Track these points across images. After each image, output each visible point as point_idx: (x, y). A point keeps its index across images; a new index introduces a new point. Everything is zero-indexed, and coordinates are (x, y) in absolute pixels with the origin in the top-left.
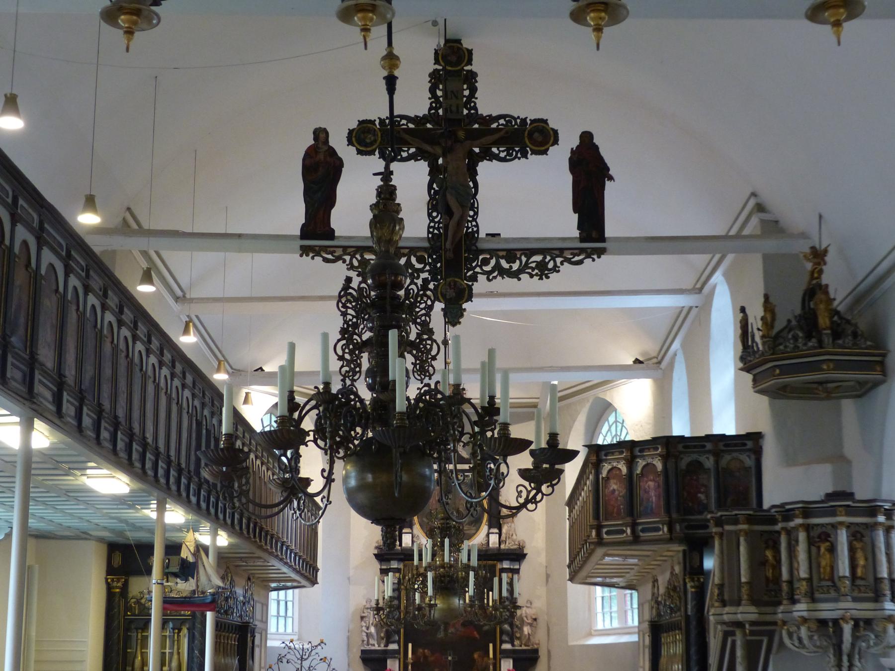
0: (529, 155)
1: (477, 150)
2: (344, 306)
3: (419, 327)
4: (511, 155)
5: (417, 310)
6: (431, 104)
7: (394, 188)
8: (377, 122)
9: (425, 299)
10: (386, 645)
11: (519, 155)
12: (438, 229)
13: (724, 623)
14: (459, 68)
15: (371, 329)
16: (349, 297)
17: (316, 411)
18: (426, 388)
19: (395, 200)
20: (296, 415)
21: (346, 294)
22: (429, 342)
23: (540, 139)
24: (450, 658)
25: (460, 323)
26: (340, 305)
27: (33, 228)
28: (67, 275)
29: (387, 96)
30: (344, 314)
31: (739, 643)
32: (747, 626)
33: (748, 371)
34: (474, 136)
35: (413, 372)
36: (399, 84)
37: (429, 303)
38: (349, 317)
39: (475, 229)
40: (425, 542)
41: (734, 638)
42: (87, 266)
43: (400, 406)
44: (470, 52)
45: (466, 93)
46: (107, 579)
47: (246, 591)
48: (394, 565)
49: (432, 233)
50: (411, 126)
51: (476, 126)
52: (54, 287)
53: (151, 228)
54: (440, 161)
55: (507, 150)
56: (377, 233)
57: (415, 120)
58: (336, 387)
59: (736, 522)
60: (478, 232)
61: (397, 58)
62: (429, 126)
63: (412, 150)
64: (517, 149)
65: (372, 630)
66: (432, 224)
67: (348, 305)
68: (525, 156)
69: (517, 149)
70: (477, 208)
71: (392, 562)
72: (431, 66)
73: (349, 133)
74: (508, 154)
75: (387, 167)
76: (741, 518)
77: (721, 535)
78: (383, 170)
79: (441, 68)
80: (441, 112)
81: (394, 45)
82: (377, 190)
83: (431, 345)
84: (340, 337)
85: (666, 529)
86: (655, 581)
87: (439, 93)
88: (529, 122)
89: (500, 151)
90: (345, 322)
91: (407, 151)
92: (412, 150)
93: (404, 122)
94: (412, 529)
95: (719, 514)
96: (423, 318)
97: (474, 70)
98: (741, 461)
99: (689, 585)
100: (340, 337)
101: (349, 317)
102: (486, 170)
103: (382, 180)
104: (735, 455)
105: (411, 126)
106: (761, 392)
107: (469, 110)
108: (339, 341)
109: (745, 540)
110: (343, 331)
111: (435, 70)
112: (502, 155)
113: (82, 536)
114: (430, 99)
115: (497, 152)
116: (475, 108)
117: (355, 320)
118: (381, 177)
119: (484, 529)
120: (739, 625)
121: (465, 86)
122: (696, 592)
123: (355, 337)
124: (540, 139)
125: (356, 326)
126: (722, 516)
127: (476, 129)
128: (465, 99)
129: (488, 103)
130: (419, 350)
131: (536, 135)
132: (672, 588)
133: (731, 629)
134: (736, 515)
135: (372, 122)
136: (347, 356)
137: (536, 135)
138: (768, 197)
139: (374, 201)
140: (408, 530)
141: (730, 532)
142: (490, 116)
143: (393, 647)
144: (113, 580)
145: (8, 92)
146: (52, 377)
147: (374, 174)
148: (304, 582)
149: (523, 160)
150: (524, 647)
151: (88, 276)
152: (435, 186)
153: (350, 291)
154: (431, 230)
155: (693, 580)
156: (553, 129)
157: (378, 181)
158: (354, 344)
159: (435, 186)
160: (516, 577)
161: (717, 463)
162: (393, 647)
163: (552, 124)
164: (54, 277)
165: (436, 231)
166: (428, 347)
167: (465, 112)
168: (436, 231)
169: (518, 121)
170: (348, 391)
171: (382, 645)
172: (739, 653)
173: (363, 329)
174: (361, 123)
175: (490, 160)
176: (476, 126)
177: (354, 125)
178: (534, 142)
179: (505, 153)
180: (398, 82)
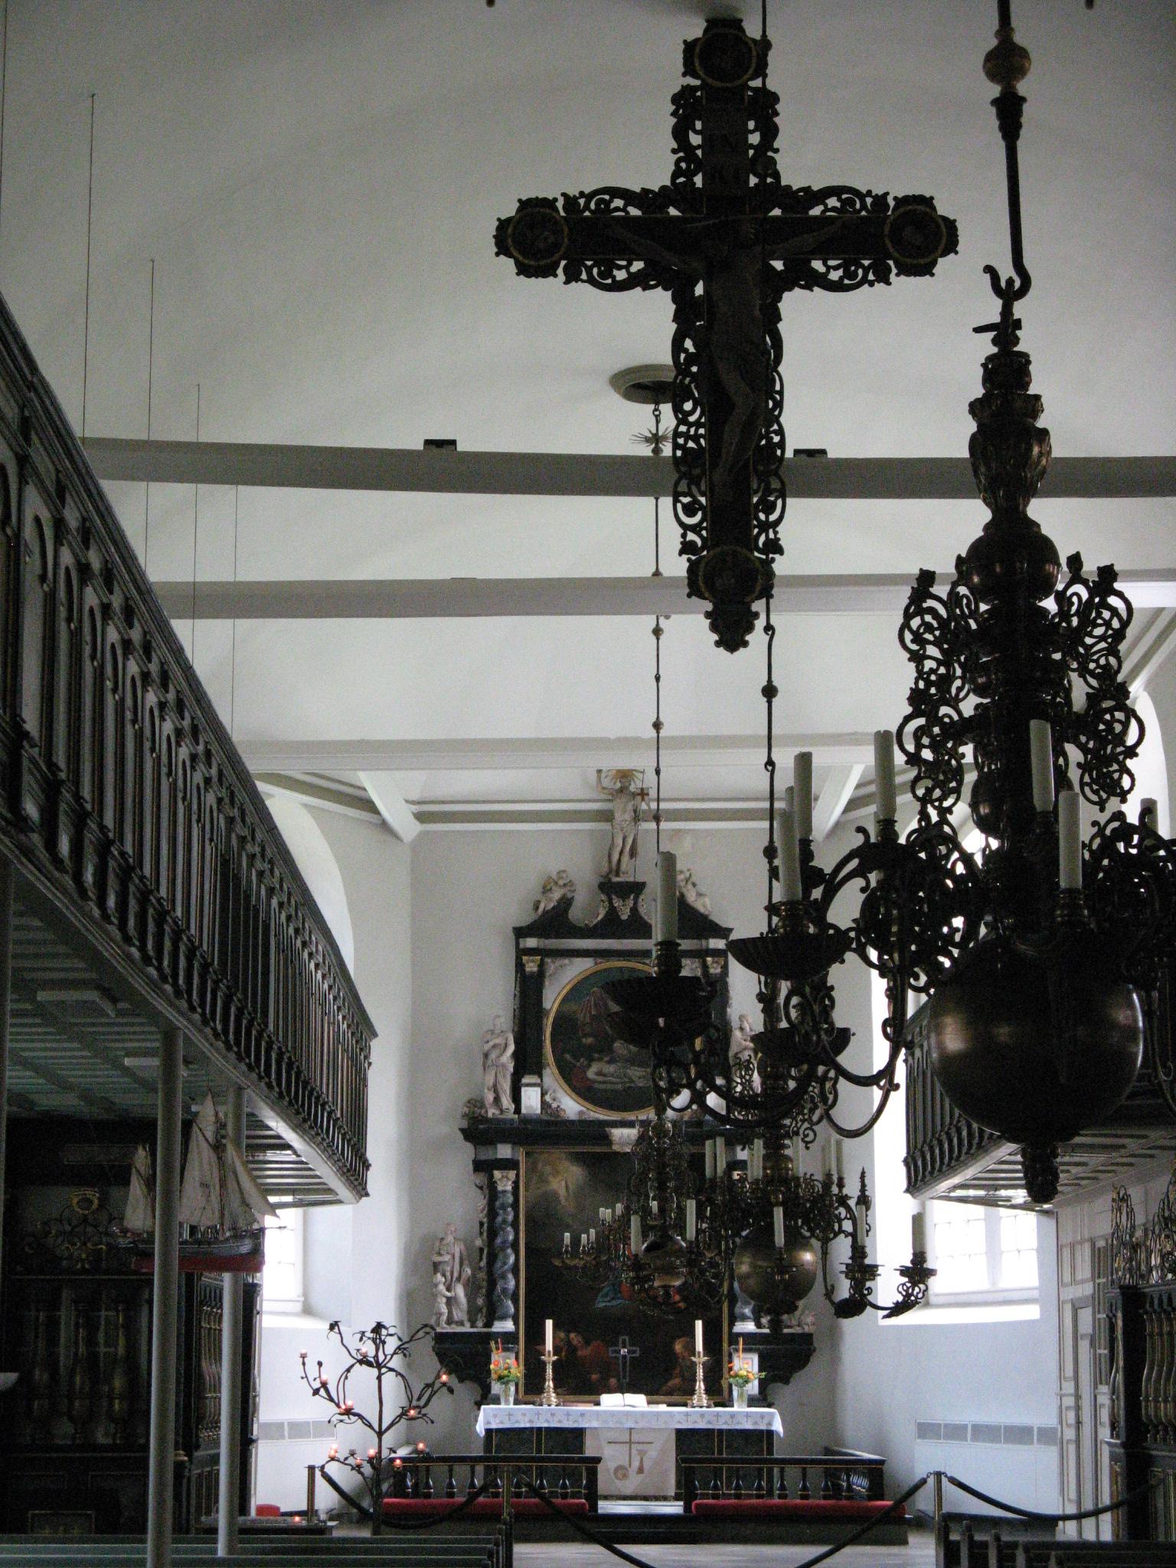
0: (893, 277)
1: (778, 265)
2: (918, 638)
3: (1094, 682)
4: (854, 275)
5: (1089, 641)
6: (677, 163)
7: (1024, 360)
8: (560, 204)
9: (1106, 614)
11: (871, 277)
12: (696, 438)
14: (740, 82)
15: (979, 691)
16: (928, 618)
17: (859, 882)
18: (1116, 824)
19: (1026, 385)
20: (817, 893)
21: (921, 612)
22: (1119, 715)
25: (745, 644)
26: (908, 636)
29: (1002, 144)
30: (917, 658)
34: (774, 236)
35: (1082, 784)
36: (1029, 114)
37: (1116, 624)
38: (929, 664)
39: (776, 439)
43: (1069, 875)
45: (755, 139)
48: (504, 1151)
49: (683, 447)
50: (634, 212)
51: (777, 212)
53: (152, 438)
54: (699, 290)
56: (989, 468)
57: (641, 199)
58: (907, 826)
60: (782, 445)
61: (1023, 53)
62: (673, 211)
63: (638, 266)
64: (866, 263)
65: (460, 1291)
66: (683, 428)
67: (929, 637)
69: (866, 263)
70: (781, 393)
71: (500, 1146)
72: (676, 79)
73: (498, 229)
74: (848, 274)
75: (1007, 311)
78: (997, 319)
79: (697, 82)
80: (698, 181)
81: (1014, 23)
82: (984, 365)
83: (1126, 725)
84: (909, 710)
87: (695, 140)
88: (892, 203)
89: (829, 268)
90: (920, 674)
91: (627, 268)
92: (638, 266)
93: (618, 203)
94: (541, 1076)
96: (1102, 661)
100: (909, 710)
101: (929, 664)
102: (799, 310)
103: (995, 342)
105: (634, 212)
108: (907, 719)
110: (917, 698)
111: (687, 90)
112: (835, 276)
114: (674, 151)
115: (822, 269)
116: (776, 175)
117: (942, 670)
118: (991, 335)
121: (751, 125)
123: (944, 710)
125: (945, 681)
127: (777, 217)
128: (751, 152)
129: (806, 158)
130: (1094, 734)
131: (908, 232)
135: (550, 203)
136: (927, 755)
137: (908, 232)
139: (979, 392)
140: (534, 1079)
142: (807, 190)
147: (977, 330)
149: (880, 287)
152: (688, 344)
153: (930, 603)
154: (681, 441)
156: (945, 219)
157: (985, 345)
158: (942, 725)
159: (688, 344)
163: (942, 209)
165: (691, 444)
166: (1118, 728)
167: (753, 181)
168: (691, 444)
169: (869, 200)
170: (936, 837)
171: (480, 1323)
173: (959, 689)
174: (524, 204)
175: (808, 287)
176: (777, 212)
177: (510, 210)
179: (840, 272)
180: (1026, 107)
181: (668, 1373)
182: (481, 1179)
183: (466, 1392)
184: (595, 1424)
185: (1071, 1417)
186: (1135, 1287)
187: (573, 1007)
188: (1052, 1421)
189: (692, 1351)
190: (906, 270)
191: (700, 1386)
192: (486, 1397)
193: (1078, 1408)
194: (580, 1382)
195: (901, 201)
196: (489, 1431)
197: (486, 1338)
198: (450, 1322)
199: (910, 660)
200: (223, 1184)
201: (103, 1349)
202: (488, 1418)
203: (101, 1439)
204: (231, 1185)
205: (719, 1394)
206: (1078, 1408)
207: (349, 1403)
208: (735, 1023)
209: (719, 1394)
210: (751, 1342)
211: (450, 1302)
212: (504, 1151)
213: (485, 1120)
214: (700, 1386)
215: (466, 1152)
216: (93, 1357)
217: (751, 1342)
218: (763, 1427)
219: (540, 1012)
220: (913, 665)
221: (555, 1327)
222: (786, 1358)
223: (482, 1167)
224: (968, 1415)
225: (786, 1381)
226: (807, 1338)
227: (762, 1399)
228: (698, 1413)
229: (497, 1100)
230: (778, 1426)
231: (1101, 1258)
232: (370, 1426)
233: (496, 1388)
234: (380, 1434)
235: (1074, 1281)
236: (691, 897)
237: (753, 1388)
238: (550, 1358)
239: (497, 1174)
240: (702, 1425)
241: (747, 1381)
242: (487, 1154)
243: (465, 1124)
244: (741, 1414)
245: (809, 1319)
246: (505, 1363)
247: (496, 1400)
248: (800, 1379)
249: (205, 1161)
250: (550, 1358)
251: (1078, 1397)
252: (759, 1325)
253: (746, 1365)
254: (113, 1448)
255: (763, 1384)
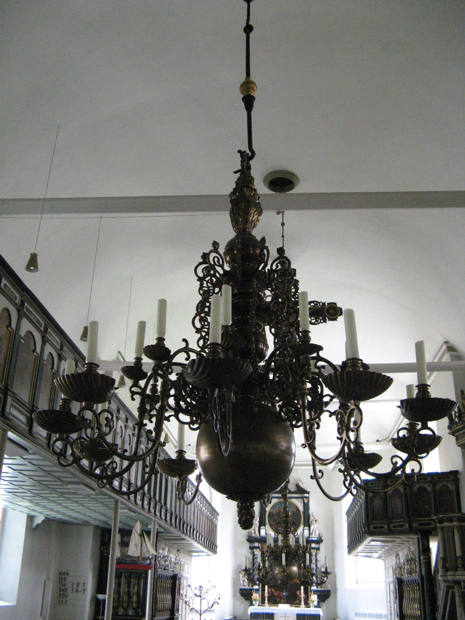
0: (327, 321)
4: (318, 321)
10: (252, 586)
13: (448, 581)
23: (333, 312)
24: (284, 594)
27: (17, 304)
28: (44, 343)
31: (457, 594)
32: (462, 584)
33: (453, 435)
36: (256, 104)
40: (272, 534)
41: (453, 590)
42: (61, 342)
44: (295, 270)
45: (293, 290)
46: (100, 548)
47: (176, 557)
48: (256, 544)
52: (33, 348)
55: (316, 319)
59: (451, 520)
68: (325, 321)
76: (454, 519)
77: (442, 528)
78: (240, 168)
85: (407, 526)
86: (397, 555)
88: (326, 304)
95: (441, 516)
97: (297, 279)
98: (447, 487)
99: (422, 558)
104: (444, 483)
106: (459, 446)
107: (295, 299)
109: (458, 531)
113: (86, 524)
119: (302, 527)
120: (458, 582)
122: (426, 562)
124: (333, 312)
126: (442, 517)
131: (331, 310)
132: (409, 561)
133: (451, 585)
134: (451, 516)
137: (331, 310)
138: (456, 342)
141: (448, 527)
143: (256, 587)
144: (104, 549)
145: (33, 252)
146: (26, 407)
148: (210, 553)
150: (322, 589)
151: (62, 349)
155: (425, 555)
160: (318, 551)
161: (434, 488)
162: (256, 587)
163: (339, 305)
164: (33, 343)
171: (250, 586)
172: (457, 600)
178: (329, 314)
181: (295, 600)
182: (251, 551)
183: (248, 603)
184: (277, 612)
185: (389, 613)
186: (401, 578)
187: (272, 510)
188: (386, 613)
189: (300, 593)
190: (331, 319)
191: (303, 603)
192: (251, 604)
193: (391, 610)
194: (274, 601)
195: (328, 304)
196: (251, 613)
197: (253, 589)
198: (243, 585)
199: (198, 280)
200: (142, 545)
201: (132, 590)
202: (252, 609)
203: (131, 614)
204: (144, 545)
205: (307, 604)
206: (391, 610)
207: (194, 607)
208: (311, 514)
209: (307, 604)
210: (315, 592)
211: (243, 581)
212: (256, 544)
213: (252, 537)
214: (303, 603)
215: (248, 545)
216: (129, 592)
217: (315, 592)
218: (317, 613)
219: (265, 511)
220: (199, 283)
221: (268, 588)
222: (324, 596)
223: (252, 548)
224: (367, 612)
225: (324, 601)
226: (329, 591)
227: (318, 606)
228: (302, 609)
229: (255, 532)
230: (321, 613)
231: (394, 570)
232: (197, 612)
233: (254, 602)
234: (201, 615)
235: (389, 577)
236: (300, 484)
237: (316, 603)
238: (266, 595)
239: (255, 550)
240: (303, 613)
241: (314, 602)
242: (252, 545)
243: (247, 538)
244: (312, 610)
245: (329, 586)
246: (256, 596)
247: (254, 605)
248: (327, 601)
249: (136, 539)
250: (266, 595)
251: (391, 607)
252: (317, 588)
253: (314, 598)
254: (133, 616)
255: (318, 602)
